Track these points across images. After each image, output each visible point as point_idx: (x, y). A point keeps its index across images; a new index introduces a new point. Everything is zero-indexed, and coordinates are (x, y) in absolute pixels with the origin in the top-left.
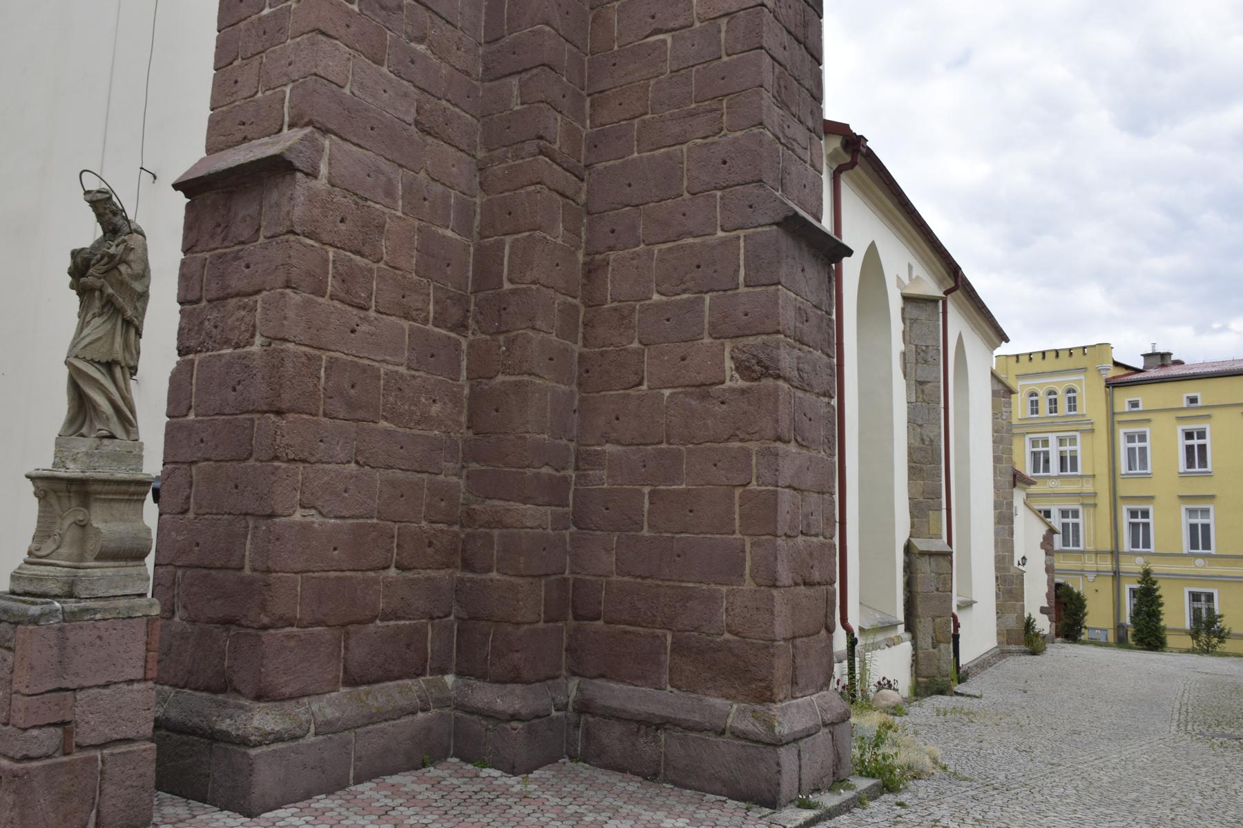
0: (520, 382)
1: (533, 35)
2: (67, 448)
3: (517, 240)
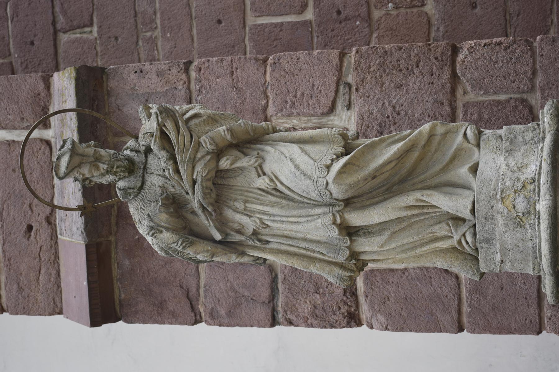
1: (17, 16)
2: (497, 182)
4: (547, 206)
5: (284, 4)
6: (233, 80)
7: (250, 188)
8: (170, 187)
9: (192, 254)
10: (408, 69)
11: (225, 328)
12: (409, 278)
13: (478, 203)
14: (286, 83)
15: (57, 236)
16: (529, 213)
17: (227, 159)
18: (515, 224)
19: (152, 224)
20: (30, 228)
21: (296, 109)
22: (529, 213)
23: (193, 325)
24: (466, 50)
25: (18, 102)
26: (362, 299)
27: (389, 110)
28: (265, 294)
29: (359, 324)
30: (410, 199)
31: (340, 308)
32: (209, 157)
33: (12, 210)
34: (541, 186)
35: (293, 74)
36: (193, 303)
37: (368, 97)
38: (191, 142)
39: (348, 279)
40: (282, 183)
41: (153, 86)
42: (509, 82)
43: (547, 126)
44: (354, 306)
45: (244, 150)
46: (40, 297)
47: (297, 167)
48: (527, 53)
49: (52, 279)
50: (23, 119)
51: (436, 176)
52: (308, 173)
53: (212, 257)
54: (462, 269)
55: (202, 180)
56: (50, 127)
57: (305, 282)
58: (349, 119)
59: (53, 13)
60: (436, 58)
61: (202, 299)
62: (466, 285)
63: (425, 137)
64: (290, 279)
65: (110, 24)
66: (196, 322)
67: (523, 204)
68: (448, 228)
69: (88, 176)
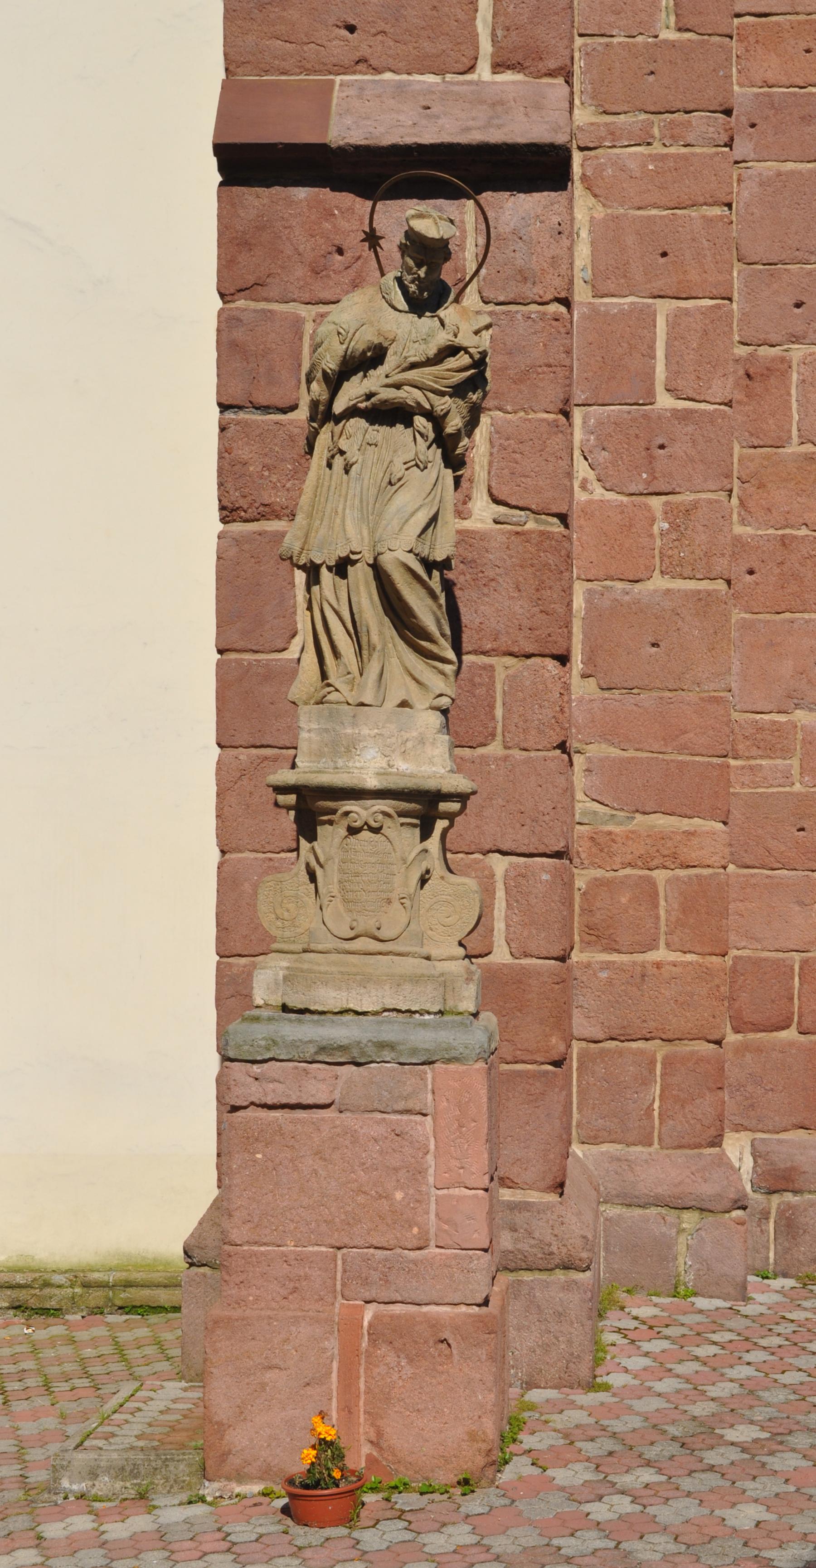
0: (709, 593)
3: (687, 312)
5: (681, 362)
6: (540, 366)
10: (539, 599)
11: (215, 338)
15: (339, 74)
21: (498, 452)
25: (531, 22)
27: (490, 573)
28: (262, 400)
35: (542, 450)
37: (508, 548)
41: (539, 250)
42: (516, 721)
45: (434, 446)
49: (277, 62)
50: (508, 30)
56: (494, 73)
58: (482, 521)
60: (549, 635)
61: (252, 305)
64: (281, 432)
65: (676, 64)
66: (222, 295)
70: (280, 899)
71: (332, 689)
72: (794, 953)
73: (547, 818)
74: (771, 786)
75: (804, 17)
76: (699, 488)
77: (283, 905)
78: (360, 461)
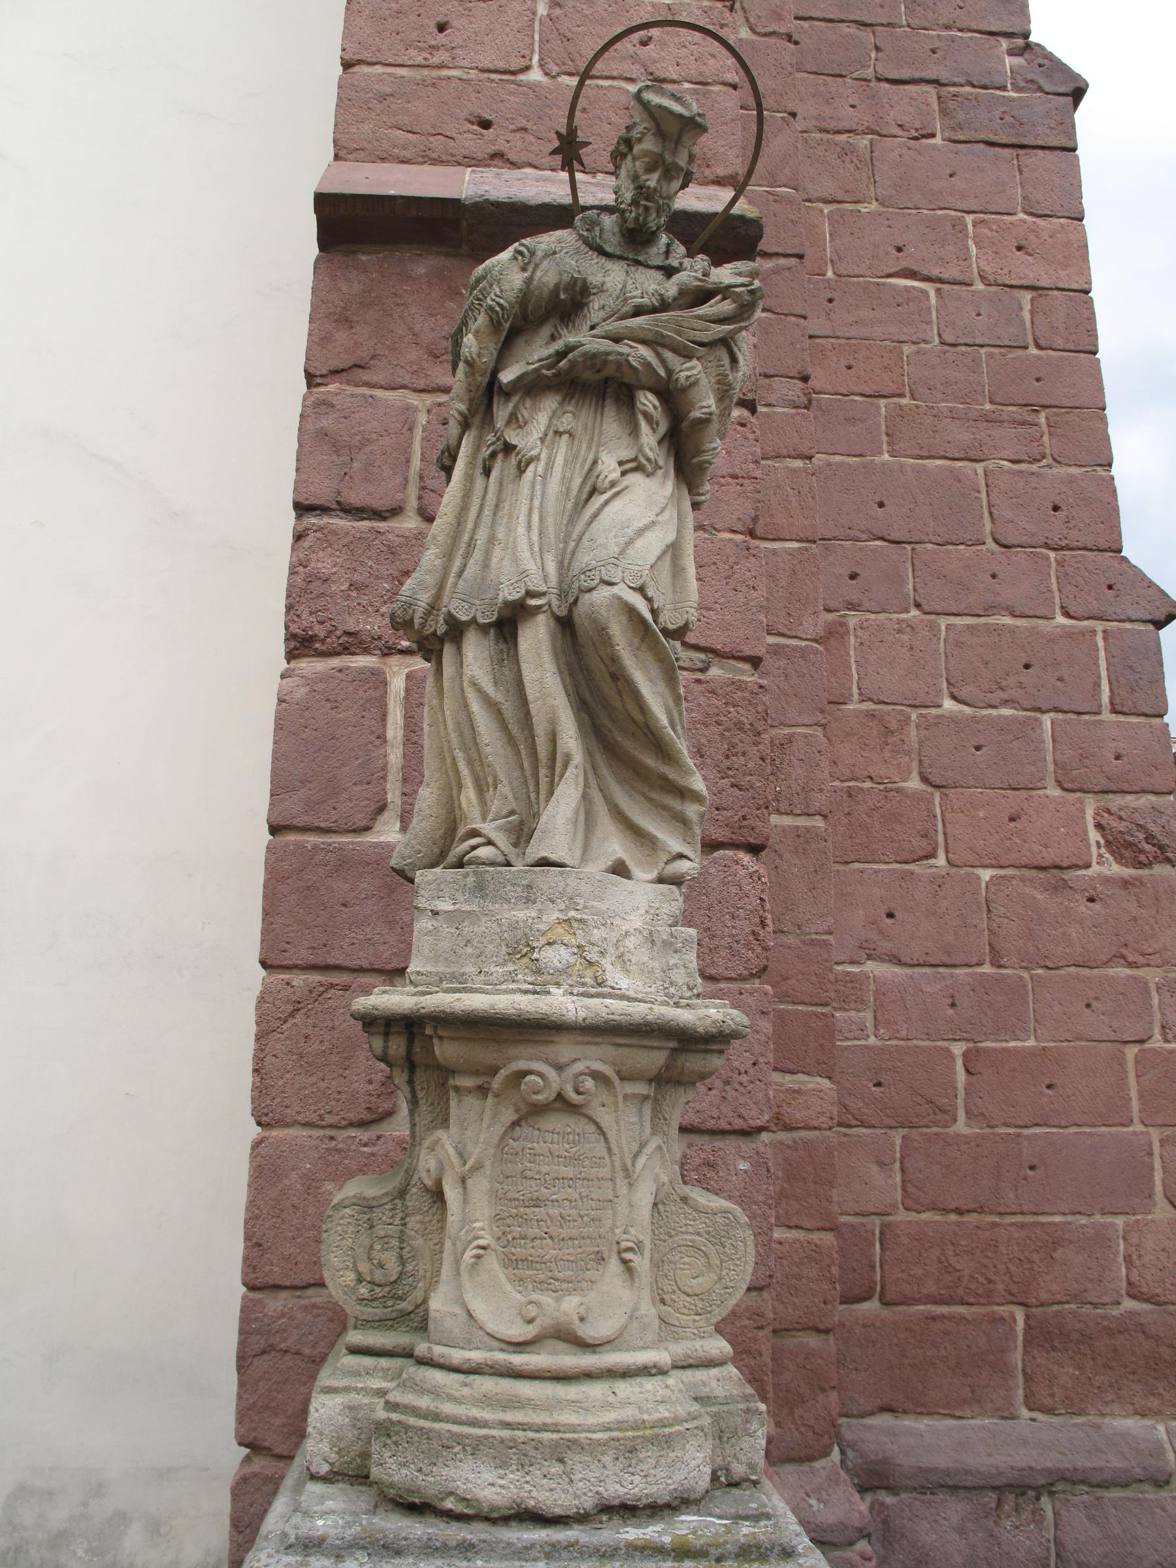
2: (599, 913)
4: (564, 1012)
6: (723, 477)
7: (598, 446)
8: (602, 302)
9: (473, 326)
10: (729, 769)
12: (370, 746)
13: (562, 873)
14: (715, 564)
16: (538, 972)
17: (655, 407)
18: (517, 942)
19: (540, 254)
20: (486, 124)
22: (538, 972)
23: (306, 371)
24: (756, 868)
26: (335, 662)
28: (354, 498)
29: (291, 656)
30: (571, 740)
31: (322, 623)
32: (662, 373)
33: (517, 100)
34: (601, 1000)
36: (345, 374)
38: (693, 342)
39: (408, 618)
40: (607, 503)
43: (702, 1012)
44: (324, 648)
46: (366, 128)
47: (641, 532)
48: (746, 968)
49: (396, 151)
51: (604, 796)
52: (630, 551)
53: (467, 362)
54: (416, 836)
55: (621, 354)
57: (371, 567)
59: (777, 255)
60: (744, 818)
61: (350, 389)
62: (353, 843)
63: (682, 781)
64: (377, 542)
67: (555, 961)
68: (505, 812)
69: (637, 149)
70: (367, 1242)
71: (478, 840)
72: (873, 1217)
73: (744, 1078)
74: (847, 1039)
75: (844, 341)
76: (792, 722)
77: (374, 1254)
78: (543, 456)
